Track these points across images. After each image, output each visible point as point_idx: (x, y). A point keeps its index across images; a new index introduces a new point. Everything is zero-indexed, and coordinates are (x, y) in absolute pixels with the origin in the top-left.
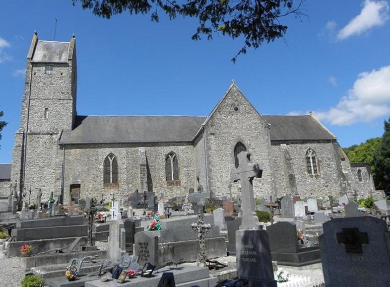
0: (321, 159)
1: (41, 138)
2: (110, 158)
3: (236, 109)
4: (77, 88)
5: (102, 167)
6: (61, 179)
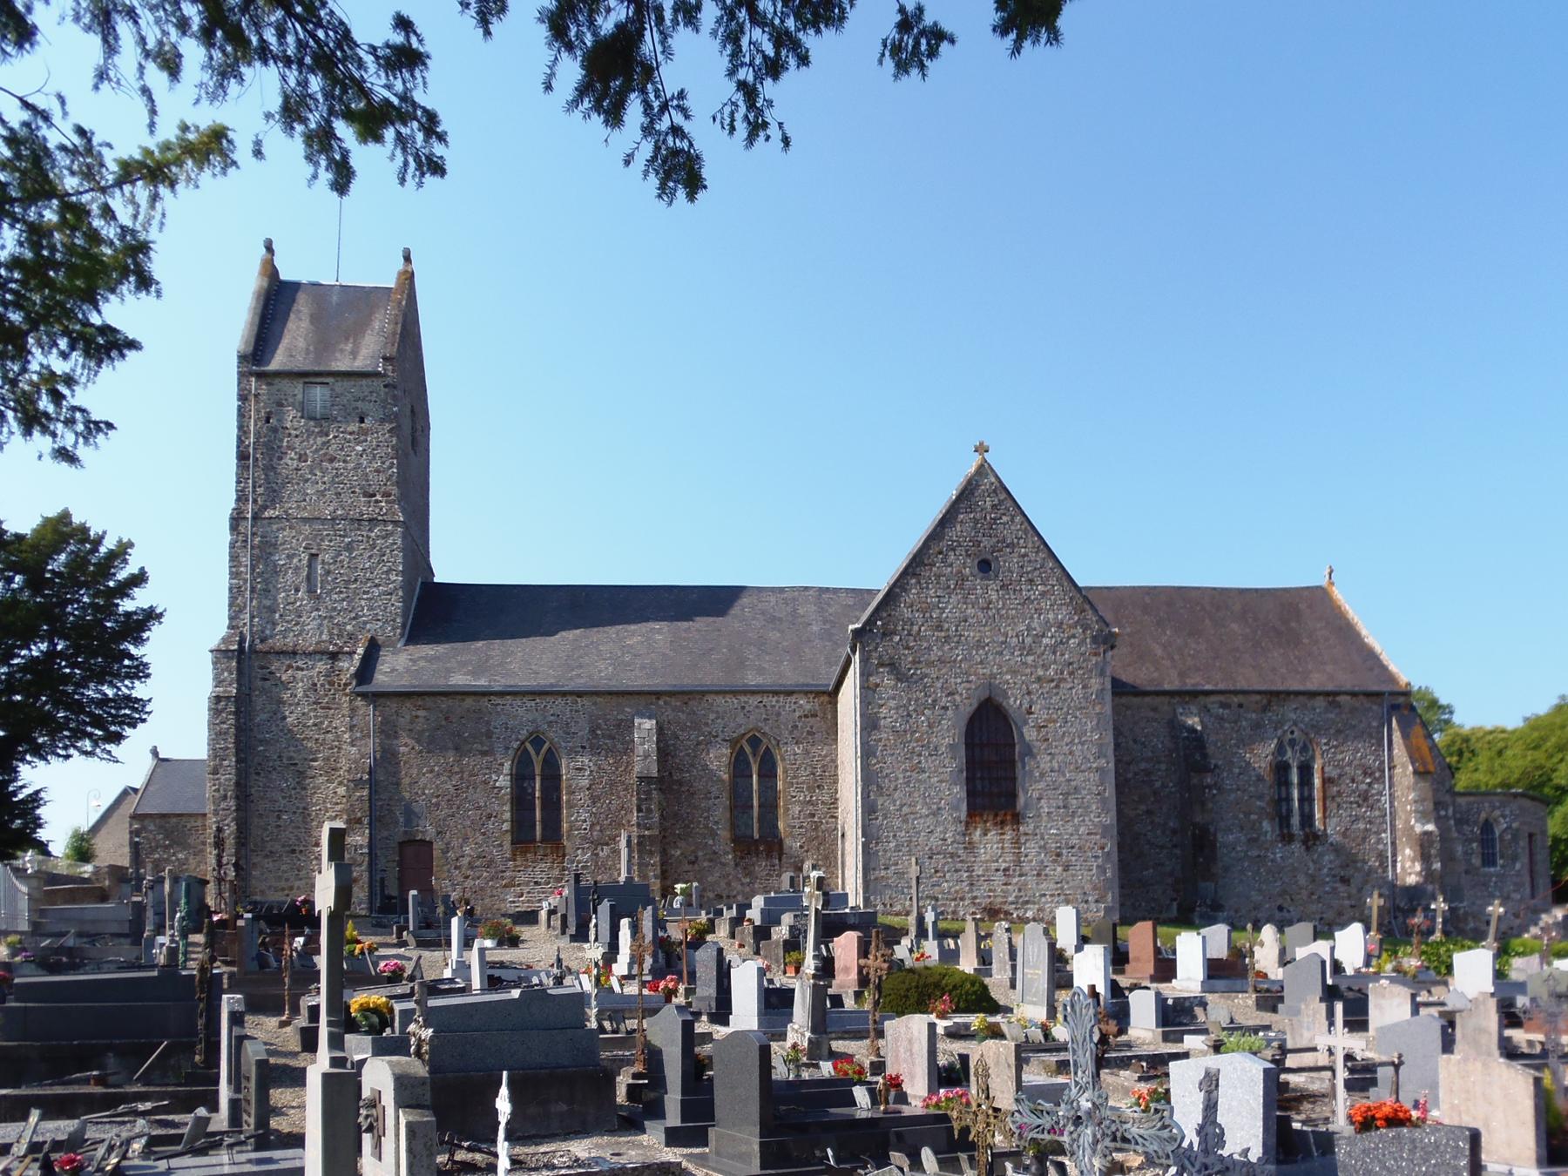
1: (299, 669)
2: (532, 752)
3: (985, 566)
4: (1303, 585)
6: (366, 821)
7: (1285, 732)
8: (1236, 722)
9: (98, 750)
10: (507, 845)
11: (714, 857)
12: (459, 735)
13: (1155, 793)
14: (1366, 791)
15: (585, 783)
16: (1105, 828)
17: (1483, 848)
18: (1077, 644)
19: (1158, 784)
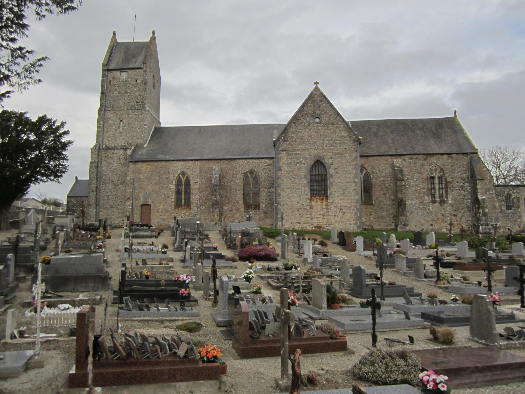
0: (450, 180)
5: (173, 187)
6: (131, 198)
7: (433, 167)
8: (415, 164)
9: (55, 179)
10: (173, 206)
11: (238, 209)
12: (160, 173)
13: (386, 188)
14: (463, 186)
15: (197, 186)
16: (357, 200)
17: (506, 204)
18: (348, 143)
19: (387, 185)
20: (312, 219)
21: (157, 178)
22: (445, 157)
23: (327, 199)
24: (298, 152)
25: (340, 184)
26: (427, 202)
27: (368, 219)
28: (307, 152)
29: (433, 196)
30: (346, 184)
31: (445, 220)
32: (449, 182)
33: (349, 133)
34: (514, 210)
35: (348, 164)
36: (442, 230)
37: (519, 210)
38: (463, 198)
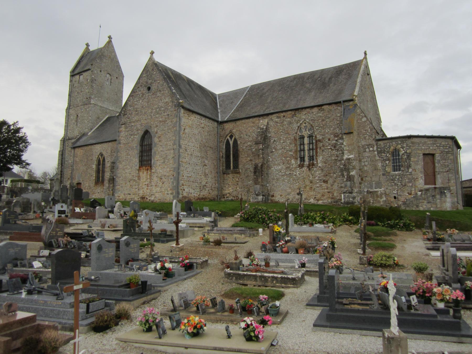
0: (321, 138)
3: (149, 89)
5: (94, 167)
6: (70, 178)
10: (94, 184)
14: (336, 144)
20: (139, 190)
21: (86, 160)
22: (315, 110)
23: (151, 169)
24: (133, 124)
25: (162, 152)
26: (294, 166)
27: (235, 189)
28: (140, 123)
29: (302, 159)
30: (166, 152)
31: (314, 187)
32: (320, 141)
33: (172, 98)
34: (403, 171)
35: (169, 131)
36: (310, 199)
37: (410, 170)
38: (335, 160)
